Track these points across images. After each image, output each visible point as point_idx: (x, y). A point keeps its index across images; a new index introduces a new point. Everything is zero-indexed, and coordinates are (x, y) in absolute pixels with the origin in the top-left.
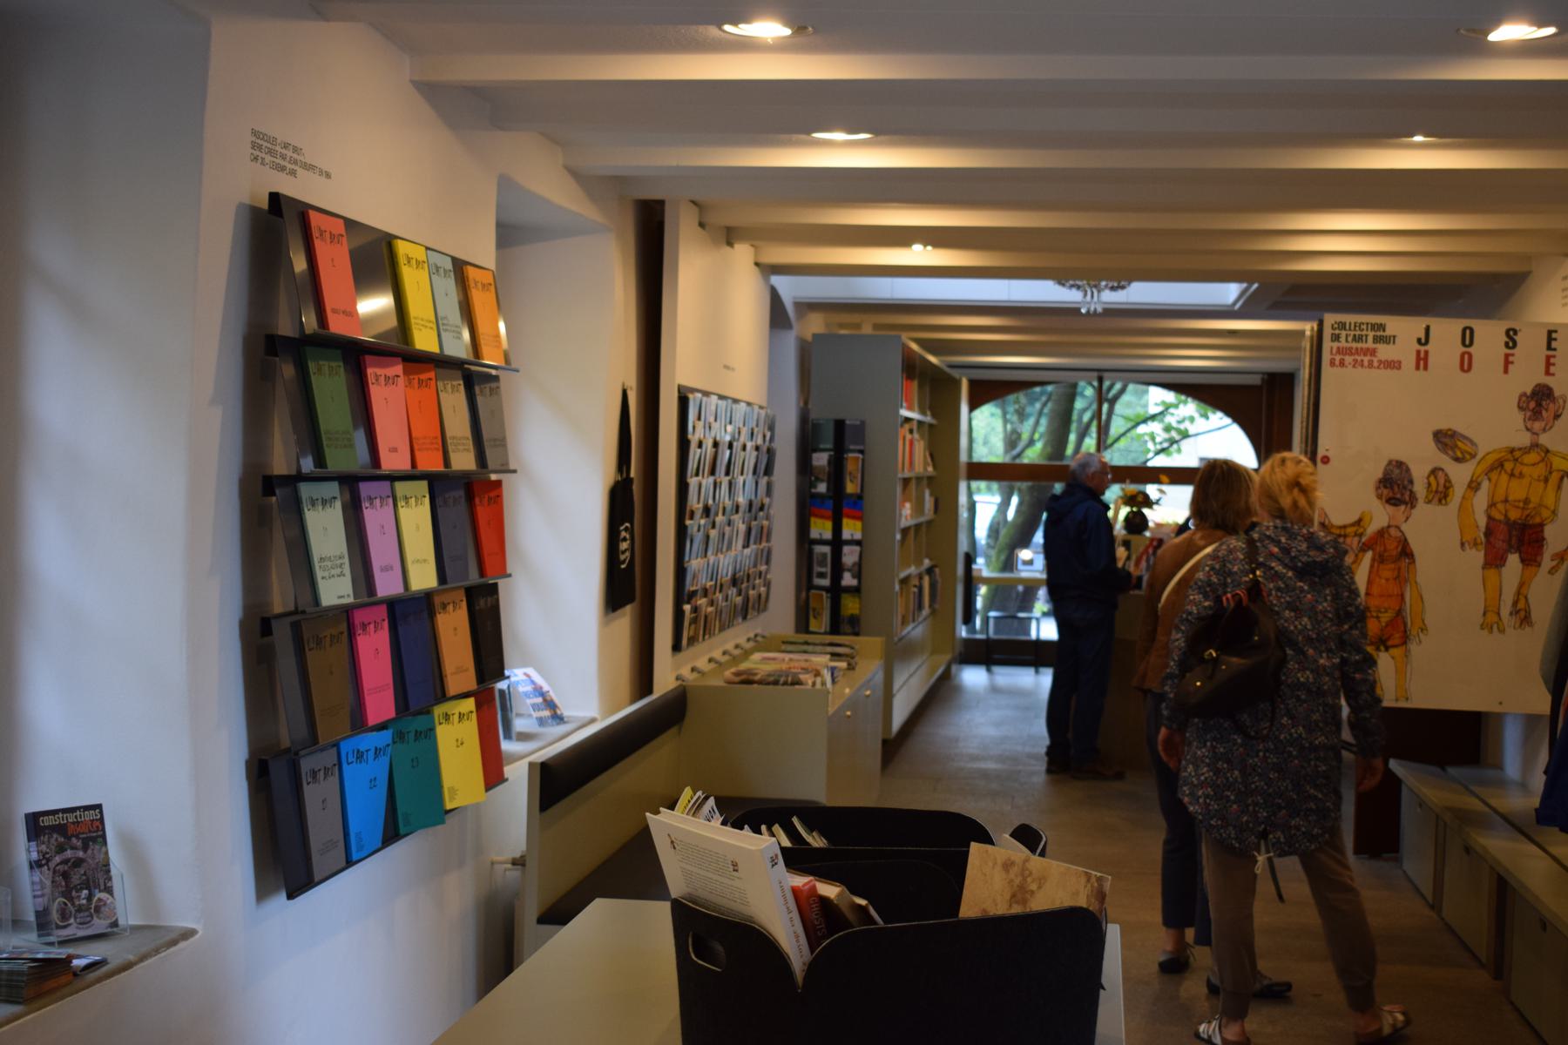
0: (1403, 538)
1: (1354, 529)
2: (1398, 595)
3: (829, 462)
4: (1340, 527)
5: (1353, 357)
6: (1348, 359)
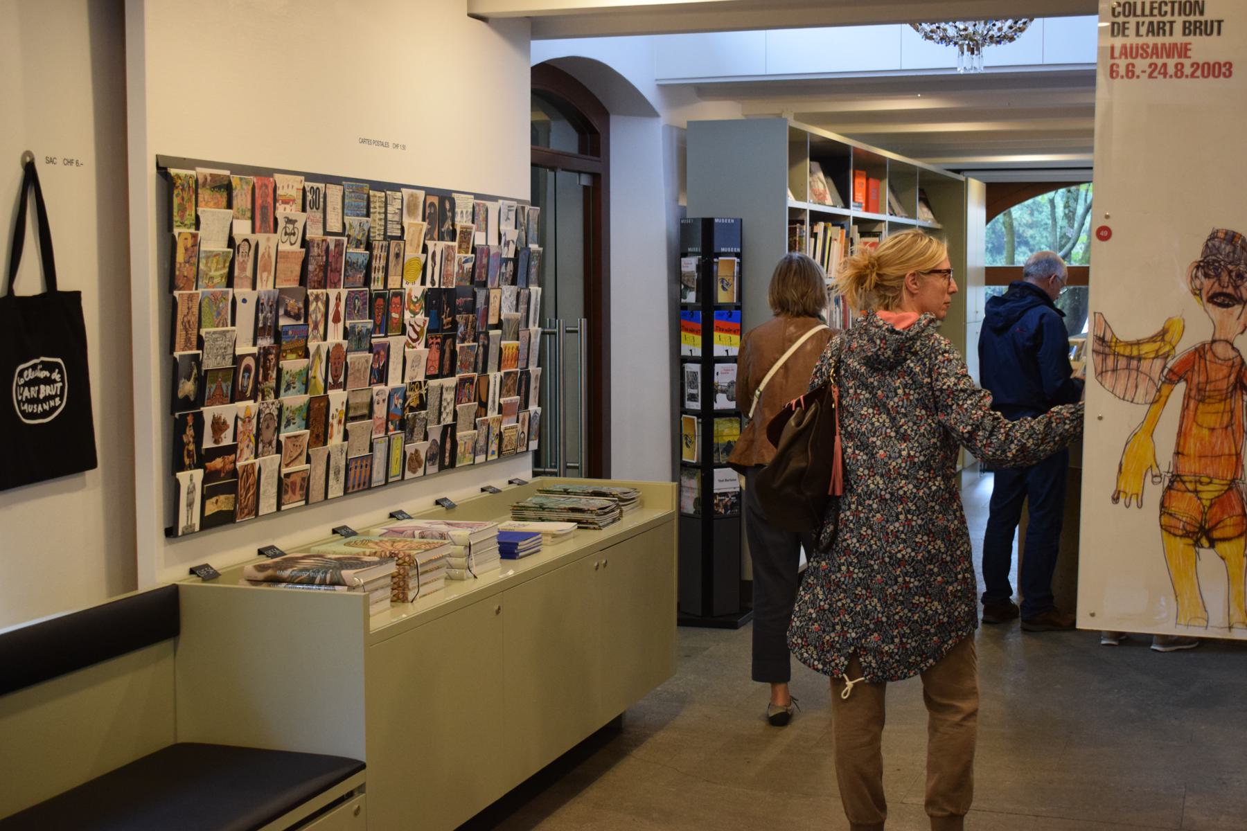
0: (1237, 360)
1: (1156, 346)
2: (1230, 455)
3: (698, 267)
4: (1131, 344)
5: (1149, 61)
6: (1141, 64)
